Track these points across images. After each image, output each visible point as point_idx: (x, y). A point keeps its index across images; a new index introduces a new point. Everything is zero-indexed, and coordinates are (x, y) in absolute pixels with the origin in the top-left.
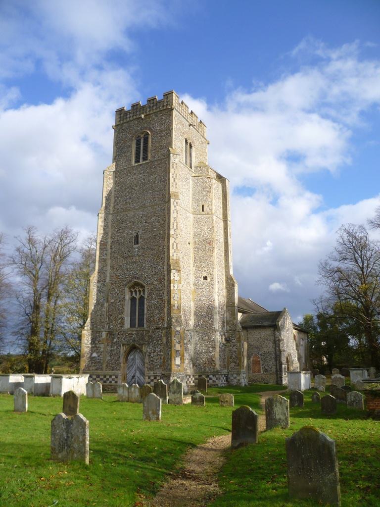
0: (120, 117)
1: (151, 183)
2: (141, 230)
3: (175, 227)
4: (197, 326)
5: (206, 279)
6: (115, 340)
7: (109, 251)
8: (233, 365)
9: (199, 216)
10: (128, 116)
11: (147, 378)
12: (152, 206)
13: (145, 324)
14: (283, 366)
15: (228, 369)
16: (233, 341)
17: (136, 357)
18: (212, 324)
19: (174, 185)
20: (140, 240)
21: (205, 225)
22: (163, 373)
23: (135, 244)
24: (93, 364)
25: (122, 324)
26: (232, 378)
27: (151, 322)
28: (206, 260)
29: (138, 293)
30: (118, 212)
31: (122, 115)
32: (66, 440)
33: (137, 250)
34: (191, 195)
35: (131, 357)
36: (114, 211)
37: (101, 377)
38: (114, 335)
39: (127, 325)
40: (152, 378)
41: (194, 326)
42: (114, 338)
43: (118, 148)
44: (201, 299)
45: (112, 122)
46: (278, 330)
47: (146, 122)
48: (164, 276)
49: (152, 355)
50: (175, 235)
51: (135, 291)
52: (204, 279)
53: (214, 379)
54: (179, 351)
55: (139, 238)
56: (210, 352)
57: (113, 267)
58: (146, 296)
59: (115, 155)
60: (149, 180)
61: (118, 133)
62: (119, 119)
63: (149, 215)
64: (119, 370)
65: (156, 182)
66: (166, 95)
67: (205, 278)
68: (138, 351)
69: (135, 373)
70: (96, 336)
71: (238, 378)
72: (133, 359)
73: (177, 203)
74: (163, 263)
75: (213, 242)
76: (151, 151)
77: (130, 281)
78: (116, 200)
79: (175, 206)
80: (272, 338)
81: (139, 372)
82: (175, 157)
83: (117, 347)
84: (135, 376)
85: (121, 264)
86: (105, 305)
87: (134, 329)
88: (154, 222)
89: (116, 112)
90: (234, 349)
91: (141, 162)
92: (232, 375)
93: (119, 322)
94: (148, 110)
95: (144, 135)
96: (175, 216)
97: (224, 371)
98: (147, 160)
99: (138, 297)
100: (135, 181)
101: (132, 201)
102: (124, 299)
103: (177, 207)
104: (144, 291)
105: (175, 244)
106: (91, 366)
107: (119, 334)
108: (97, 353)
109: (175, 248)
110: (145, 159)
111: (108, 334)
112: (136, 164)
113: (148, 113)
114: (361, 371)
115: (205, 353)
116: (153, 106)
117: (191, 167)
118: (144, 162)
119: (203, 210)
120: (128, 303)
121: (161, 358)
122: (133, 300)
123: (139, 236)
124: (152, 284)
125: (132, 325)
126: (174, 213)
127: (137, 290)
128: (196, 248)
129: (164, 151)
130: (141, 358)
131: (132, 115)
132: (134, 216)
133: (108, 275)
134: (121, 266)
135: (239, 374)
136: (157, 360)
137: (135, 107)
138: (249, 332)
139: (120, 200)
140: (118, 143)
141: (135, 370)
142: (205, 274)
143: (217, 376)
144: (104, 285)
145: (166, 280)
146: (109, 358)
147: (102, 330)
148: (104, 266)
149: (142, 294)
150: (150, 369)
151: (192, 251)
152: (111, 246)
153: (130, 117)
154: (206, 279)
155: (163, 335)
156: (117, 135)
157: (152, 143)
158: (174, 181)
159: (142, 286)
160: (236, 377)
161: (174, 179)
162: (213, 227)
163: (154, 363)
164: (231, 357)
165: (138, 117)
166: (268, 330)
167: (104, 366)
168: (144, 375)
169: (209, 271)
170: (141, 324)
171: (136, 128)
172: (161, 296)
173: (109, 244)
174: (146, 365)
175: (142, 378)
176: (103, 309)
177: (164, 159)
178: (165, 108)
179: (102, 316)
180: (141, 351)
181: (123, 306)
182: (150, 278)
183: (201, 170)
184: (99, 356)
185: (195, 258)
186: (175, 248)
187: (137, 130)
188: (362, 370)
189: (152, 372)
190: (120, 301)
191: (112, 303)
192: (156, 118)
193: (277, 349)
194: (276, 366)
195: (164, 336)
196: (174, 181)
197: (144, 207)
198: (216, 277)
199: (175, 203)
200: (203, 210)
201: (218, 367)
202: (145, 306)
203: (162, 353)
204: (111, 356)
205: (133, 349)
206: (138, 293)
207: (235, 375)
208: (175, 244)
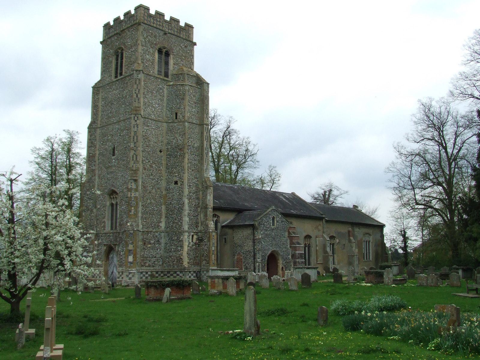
3: (135, 141)
4: (168, 227)
9: (172, 124)
14: (257, 264)
18: (181, 226)
19: (137, 100)
20: (116, 152)
21: (177, 132)
28: (177, 166)
33: (114, 160)
35: (111, 256)
37: (171, 273)
41: (165, 228)
44: (172, 203)
52: (175, 184)
53: (181, 275)
54: (131, 250)
56: (178, 251)
57: (99, 177)
67: (176, 183)
69: (113, 270)
73: (138, 117)
76: (125, 66)
79: (136, 121)
80: (252, 237)
86: (94, 211)
89: (103, 27)
90: (206, 248)
91: (119, 78)
92: (203, 271)
103: (138, 121)
105: (135, 156)
110: (121, 74)
115: (174, 252)
117: (166, 75)
119: (176, 118)
126: (134, 127)
138: (235, 231)
142: (175, 179)
143: (184, 273)
148: (92, 176)
151: (164, 158)
152: (98, 158)
158: (137, 96)
162: (185, 134)
173: (97, 155)
176: (93, 214)
182: (121, 187)
183: (178, 77)
196: (137, 96)
198: (186, 181)
199: (136, 118)
200: (176, 118)
201: (186, 264)
207: (205, 272)
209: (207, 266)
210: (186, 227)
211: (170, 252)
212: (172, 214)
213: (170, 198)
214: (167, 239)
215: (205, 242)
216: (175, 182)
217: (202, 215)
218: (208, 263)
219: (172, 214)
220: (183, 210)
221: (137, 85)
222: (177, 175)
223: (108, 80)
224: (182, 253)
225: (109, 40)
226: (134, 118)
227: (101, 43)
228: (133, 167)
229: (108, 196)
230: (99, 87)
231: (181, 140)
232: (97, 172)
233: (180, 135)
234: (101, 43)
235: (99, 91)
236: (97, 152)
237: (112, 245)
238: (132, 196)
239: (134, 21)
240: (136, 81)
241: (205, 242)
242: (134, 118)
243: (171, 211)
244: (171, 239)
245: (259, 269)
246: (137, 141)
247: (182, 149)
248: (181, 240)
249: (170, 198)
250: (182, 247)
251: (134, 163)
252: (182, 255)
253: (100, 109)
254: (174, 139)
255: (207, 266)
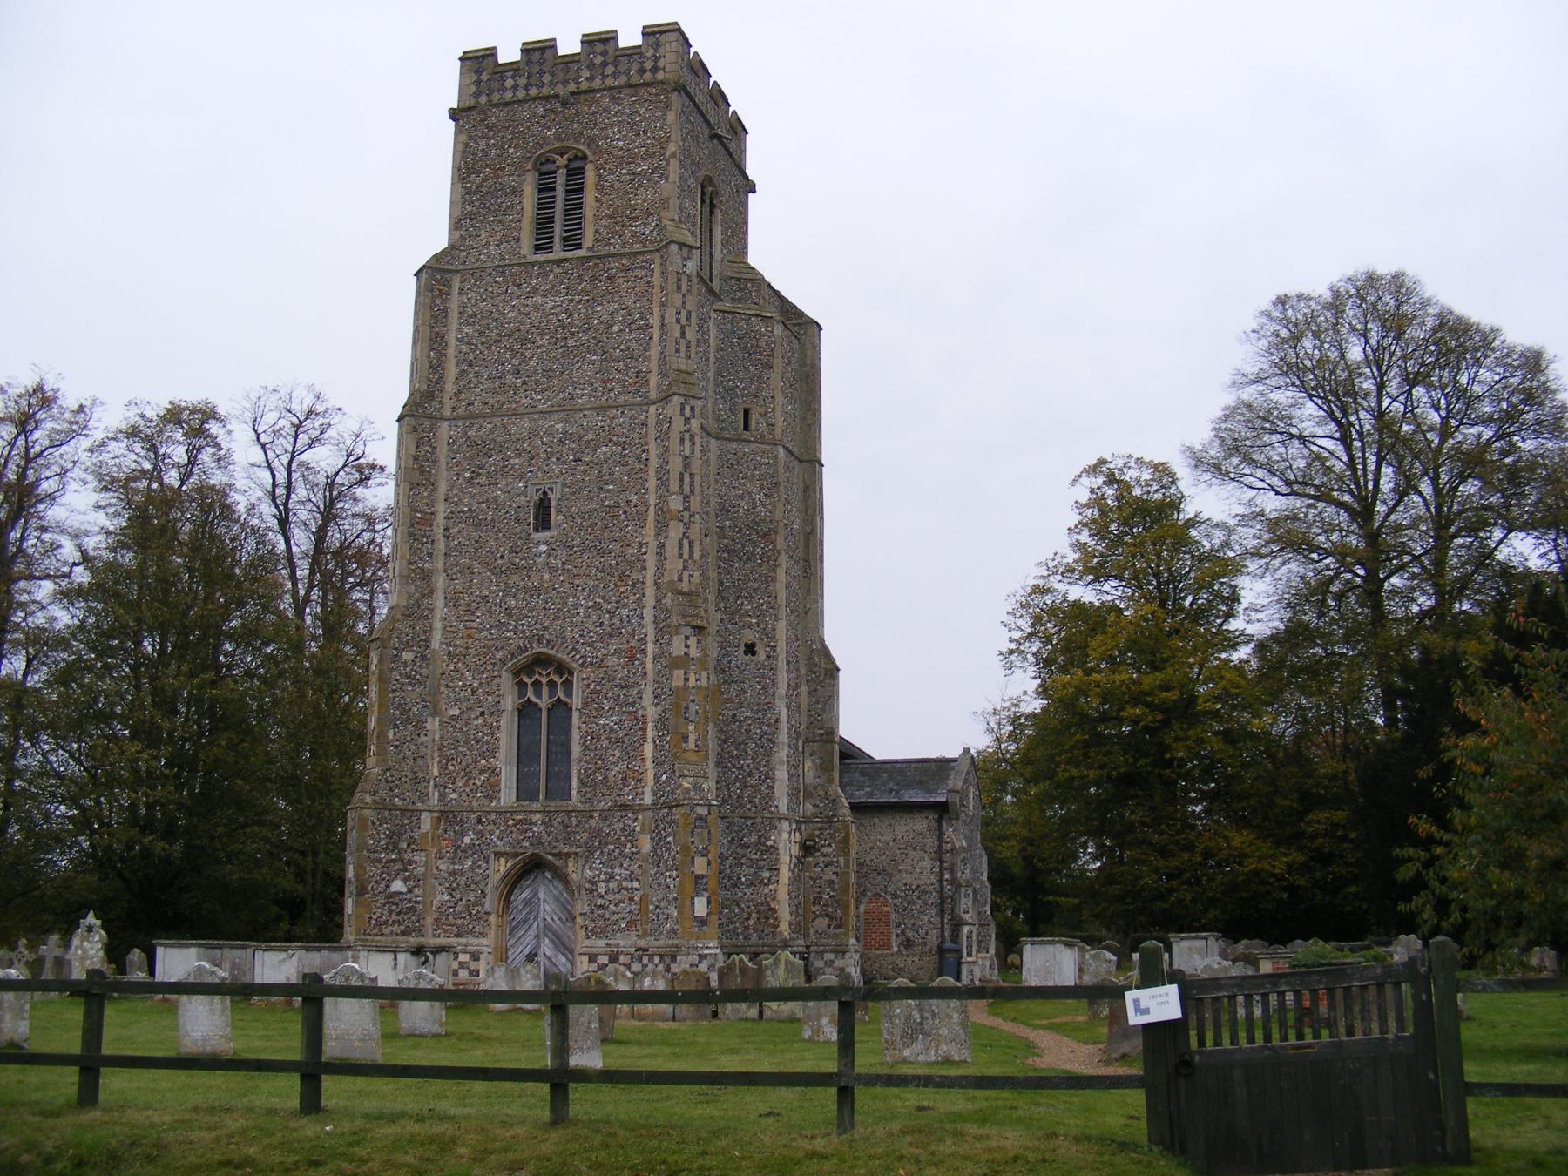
0: (478, 82)
1: (596, 330)
2: (559, 486)
3: (687, 489)
5: (754, 653)
6: (467, 840)
7: (441, 545)
8: (822, 923)
9: (734, 445)
10: (509, 83)
11: (585, 959)
12: (600, 409)
13: (574, 792)
14: (966, 929)
15: (806, 936)
16: (825, 850)
17: (544, 896)
18: (769, 797)
19: (683, 349)
20: (555, 517)
22: (642, 943)
23: (536, 530)
24: (394, 917)
25: (492, 789)
26: (820, 964)
27: (594, 785)
28: (754, 590)
29: (545, 690)
30: (472, 416)
31: (485, 77)
32: (921, 1023)
33: (543, 548)
34: (711, 375)
35: (524, 895)
36: (454, 408)
38: (462, 823)
39: (507, 795)
40: (604, 960)
42: (463, 834)
43: (469, 192)
45: (447, 90)
46: (950, 819)
47: (577, 115)
48: (643, 641)
49: (602, 891)
50: (686, 514)
51: (537, 684)
52: (746, 653)
54: (703, 876)
55: (553, 510)
57: (453, 600)
58: (576, 701)
59: (458, 214)
60: (588, 319)
61: (470, 138)
62: (473, 89)
63: (590, 437)
64: (483, 935)
65: (616, 328)
66: (654, 33)
68: (548, 875)
69: (538, 945)
70: (403, 825)
71: (839, 963)
72: (527, 902)
73: (692, 409)
74: (639, 601)
75: (776, 532)
77: (522, 650)
78: (462, 373)
79: (687, 420)
80: (931, 842)
81: (552, 941)
82: (685, 255)
83: (474, 862)
84: (536, 955)
85: (486, 592)
87: (535, 806)
88: (606, 460)
90: (829, 875)
91: (558, 253)
92: (821, 954)
93: (478, 783)
94: (586, 73)
95: (570, 160)
96: (687, 453)
97: (796, 943)
98: (579, 247)
99: (544, 702)
100: (536, 317)
101: (524, 383)
102: (497, 710)
104: (568, 684)
105: (685, 542)
106: (386, 923)
107: (479, 821)
108: (405, 880)
109: (686, 556)
110: (572, 242)
111: (439, 819)
112: (541, 258)
113: (584, 86)
114: (1204, 942)
115: (749, 886)
116: (604, 64)
118: (569, 255)
119: (746, 428)
120: (512, 721)
121: (631, 899)
122: (526, 711)
123: (553, 503)
124: (600, 664)
125: (525, 791)
127: (544, 680)
128: (726, 549)
129: (645, 225)
130: (557, 899)
131: (522, 81)
132: (533, 434)
133: (438, 625)
134: (485, 599)
135: (844, 953)
136: (616, 905)
137: (536, 56)
139: (478, 374)
140: (469, 172)
141: (537, 936)
142: (749, 636)
144: (424, 657)
145: (650, 654)
146: (446, 897)
147: (419, 805)
148: (424, 596)
149: (560, 694)
150: (591, 933)
153: (515, 88)
154: (754, 653)
155: (638, 829)
156: (466, 146)
157: (600, 188)
159: (561, 668)
160: (832, 962)
161: (683, 327)
163: (607, 916)
164: (817, 900)
165: (545, 91)
166: (919, 816)
167: (429, 921)
168: (572, 952)
169: (763, 626)
170: (559, 789)
171: (537, 130)
172: (632, 705)
173: (440, 519)
174: (579, 920)
175: (563, 959)
176: (423, 739)
177: (643, 253)
178: (648, 76)
179: (420, 762)
180: (563, 878)
181: (493, 730)
183: (741, 290)
184: (410, 891)
185: (721, 583)
186: (686, 556)
187: (545, 138)
188: (1206, 938)
189: (602, 942)
190: (482, 714)
191: (452, 718)
192: (614, 109)
193: (947, 876)
194: (942, 929)
195: (642, 832)
197: (569, 409)
199: (687, 408)
200: (746, 428)
201: (784, 927)
202: (576, 736)
203: (636, 885)
204: (451, 891)
205: (531, 867)
206: (545, 690)
207: (829, 956)
208: (685, 542)
209: (836, 936)
210: (783, 804)
211: (736, 885)
212: (738, 758)
213: (730, 700)
214: (725, 841)
215: (824, 855)
216: (746, 645)
217: (808, 764)
218: (838, 927)
219: (738, 758)
220: (774, 743)
221: (684, 296)
222: (754, 621)
223: (492, 251)
224: (775, 890)
225: (502, 113)
226: (682, 409)
227: (454, 114)
228: (680, 580)
229: (511, 676)
230: (450, 271)
231: (764, 506)
232: (440, 582)
233: (762, 487)
234: (454, 114)
235: (448, 284)
236: (441, 509)
237: (550, 858)
238: (692, 683)
239: (642, 71)
240: (679, 280)
241: (824, 855)
242: (682, 409)
243: (738, 745)
244: (738, 841)
245: (970, 947)
246: (692, 492)
247: (767, 534)
248: (772, 847)
249: (730, 700)
250: (774, 870)
251: (685, 568)
252: (774, 899)
253: (451, 352)
254: (741, 497)
255: (836, 936)
